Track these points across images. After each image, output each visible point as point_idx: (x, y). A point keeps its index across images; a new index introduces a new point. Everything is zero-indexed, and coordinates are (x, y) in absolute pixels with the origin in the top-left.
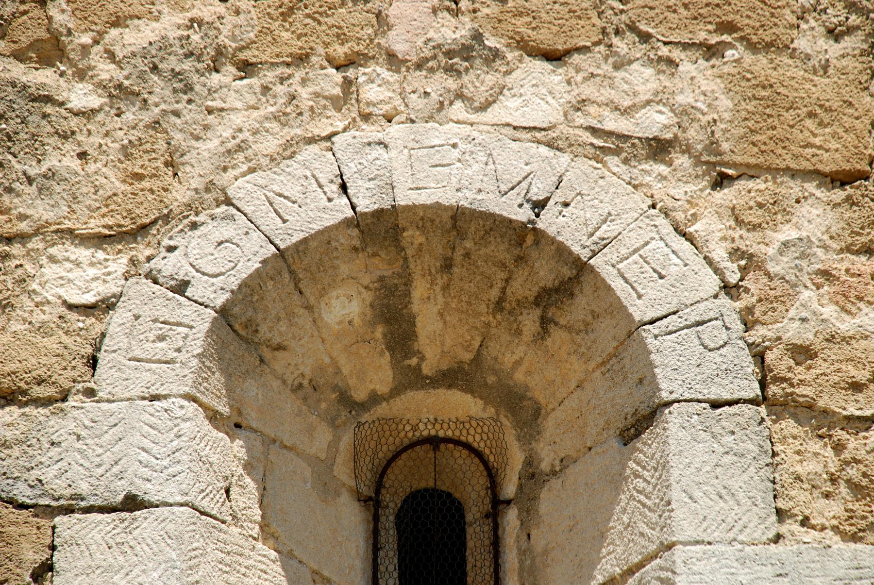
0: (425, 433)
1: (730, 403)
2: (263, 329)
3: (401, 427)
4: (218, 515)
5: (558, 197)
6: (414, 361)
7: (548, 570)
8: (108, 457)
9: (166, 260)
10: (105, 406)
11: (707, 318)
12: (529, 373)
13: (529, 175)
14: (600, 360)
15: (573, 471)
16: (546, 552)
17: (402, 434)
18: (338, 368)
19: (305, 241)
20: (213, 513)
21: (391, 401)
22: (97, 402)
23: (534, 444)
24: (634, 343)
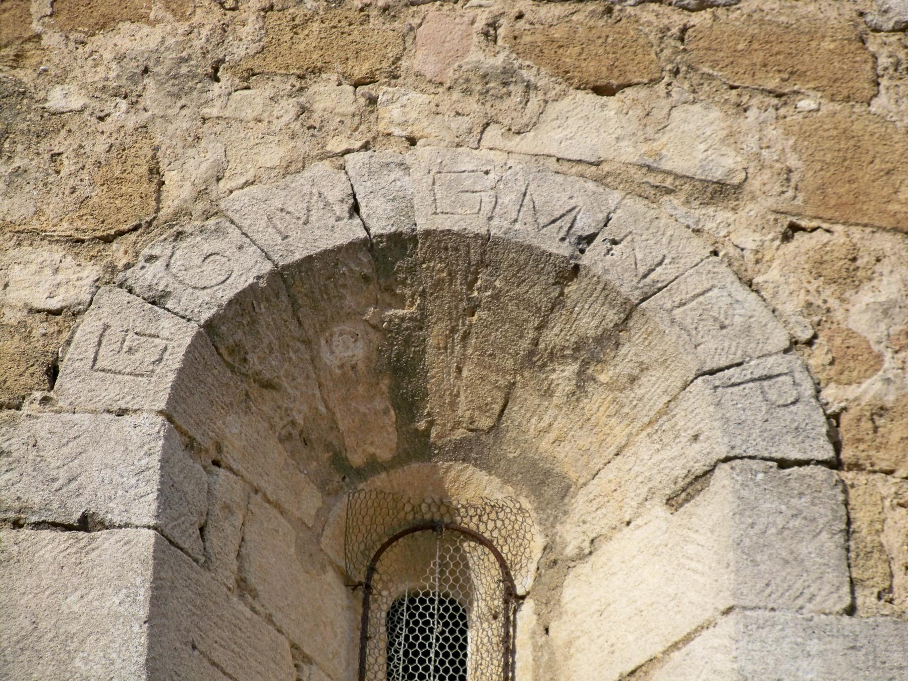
0: (428, 517)
1: (800, 463)
2: (253, 358)
3: (400, 505)
4: (190, 551)
5: (605, 234)
6: (422, 425)
7: (572, 662)
8: (63, 475)
9: (145, 270)
10: (67, 417)
11: (776, 373)
12: (558, 441)
13: (574, 208)
14: (646, 420)
15: (606, 550)
16: (569, 644)
17: (402, 514)
18: (335, 422)
19: (309, 259)
20: (186, 546)
21: (392, 472)
22: (57, 412)
23: (558, 527)
24: (691, 396)
